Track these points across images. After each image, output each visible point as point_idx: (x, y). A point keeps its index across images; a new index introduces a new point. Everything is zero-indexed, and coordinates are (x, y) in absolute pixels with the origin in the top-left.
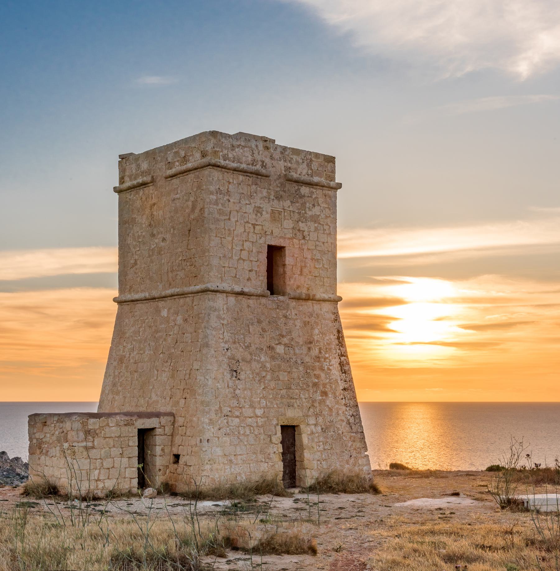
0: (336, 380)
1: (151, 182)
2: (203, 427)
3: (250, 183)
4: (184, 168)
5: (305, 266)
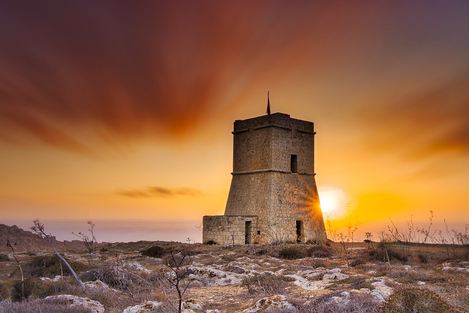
1: (248, 131)
3: (285, 132)
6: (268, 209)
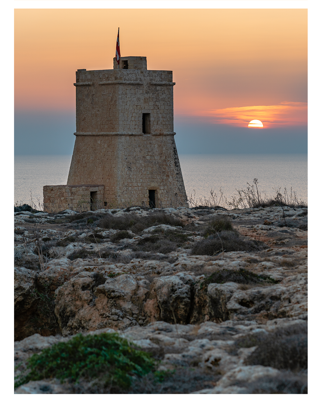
0: (173, 170)
2: (117, 191)
3: (135, 88)
4: (108, 82)
5: (159, 121)
6: (115, 177)
